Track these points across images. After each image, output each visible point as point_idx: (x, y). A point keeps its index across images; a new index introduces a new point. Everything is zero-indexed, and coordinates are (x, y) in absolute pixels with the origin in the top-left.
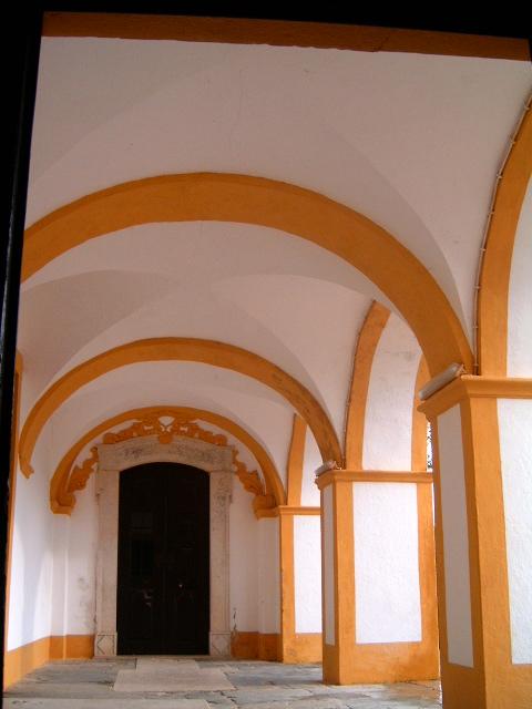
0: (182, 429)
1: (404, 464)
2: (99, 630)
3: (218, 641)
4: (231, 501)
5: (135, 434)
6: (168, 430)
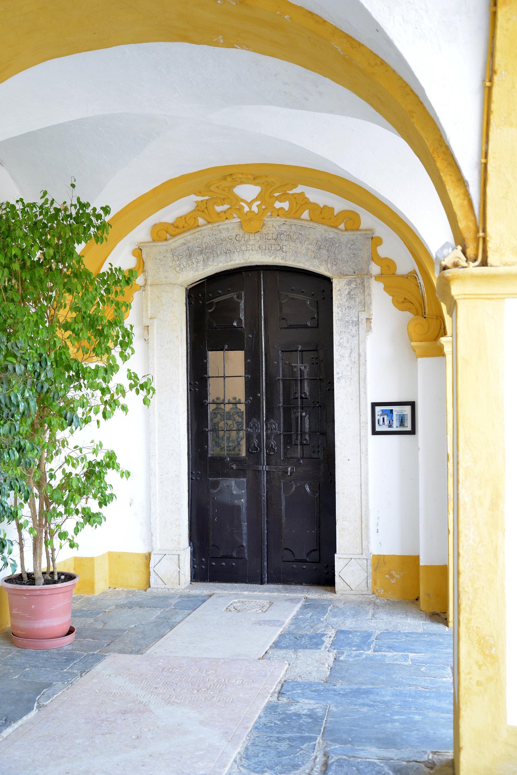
0: (278, 205)
1: (220, 432)
2: (158, 546)
3: (489, 265)
4: (369, 329)
5: (201, 221)
6: (255, 209)
